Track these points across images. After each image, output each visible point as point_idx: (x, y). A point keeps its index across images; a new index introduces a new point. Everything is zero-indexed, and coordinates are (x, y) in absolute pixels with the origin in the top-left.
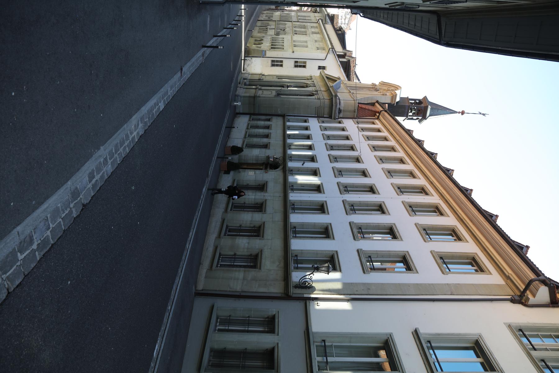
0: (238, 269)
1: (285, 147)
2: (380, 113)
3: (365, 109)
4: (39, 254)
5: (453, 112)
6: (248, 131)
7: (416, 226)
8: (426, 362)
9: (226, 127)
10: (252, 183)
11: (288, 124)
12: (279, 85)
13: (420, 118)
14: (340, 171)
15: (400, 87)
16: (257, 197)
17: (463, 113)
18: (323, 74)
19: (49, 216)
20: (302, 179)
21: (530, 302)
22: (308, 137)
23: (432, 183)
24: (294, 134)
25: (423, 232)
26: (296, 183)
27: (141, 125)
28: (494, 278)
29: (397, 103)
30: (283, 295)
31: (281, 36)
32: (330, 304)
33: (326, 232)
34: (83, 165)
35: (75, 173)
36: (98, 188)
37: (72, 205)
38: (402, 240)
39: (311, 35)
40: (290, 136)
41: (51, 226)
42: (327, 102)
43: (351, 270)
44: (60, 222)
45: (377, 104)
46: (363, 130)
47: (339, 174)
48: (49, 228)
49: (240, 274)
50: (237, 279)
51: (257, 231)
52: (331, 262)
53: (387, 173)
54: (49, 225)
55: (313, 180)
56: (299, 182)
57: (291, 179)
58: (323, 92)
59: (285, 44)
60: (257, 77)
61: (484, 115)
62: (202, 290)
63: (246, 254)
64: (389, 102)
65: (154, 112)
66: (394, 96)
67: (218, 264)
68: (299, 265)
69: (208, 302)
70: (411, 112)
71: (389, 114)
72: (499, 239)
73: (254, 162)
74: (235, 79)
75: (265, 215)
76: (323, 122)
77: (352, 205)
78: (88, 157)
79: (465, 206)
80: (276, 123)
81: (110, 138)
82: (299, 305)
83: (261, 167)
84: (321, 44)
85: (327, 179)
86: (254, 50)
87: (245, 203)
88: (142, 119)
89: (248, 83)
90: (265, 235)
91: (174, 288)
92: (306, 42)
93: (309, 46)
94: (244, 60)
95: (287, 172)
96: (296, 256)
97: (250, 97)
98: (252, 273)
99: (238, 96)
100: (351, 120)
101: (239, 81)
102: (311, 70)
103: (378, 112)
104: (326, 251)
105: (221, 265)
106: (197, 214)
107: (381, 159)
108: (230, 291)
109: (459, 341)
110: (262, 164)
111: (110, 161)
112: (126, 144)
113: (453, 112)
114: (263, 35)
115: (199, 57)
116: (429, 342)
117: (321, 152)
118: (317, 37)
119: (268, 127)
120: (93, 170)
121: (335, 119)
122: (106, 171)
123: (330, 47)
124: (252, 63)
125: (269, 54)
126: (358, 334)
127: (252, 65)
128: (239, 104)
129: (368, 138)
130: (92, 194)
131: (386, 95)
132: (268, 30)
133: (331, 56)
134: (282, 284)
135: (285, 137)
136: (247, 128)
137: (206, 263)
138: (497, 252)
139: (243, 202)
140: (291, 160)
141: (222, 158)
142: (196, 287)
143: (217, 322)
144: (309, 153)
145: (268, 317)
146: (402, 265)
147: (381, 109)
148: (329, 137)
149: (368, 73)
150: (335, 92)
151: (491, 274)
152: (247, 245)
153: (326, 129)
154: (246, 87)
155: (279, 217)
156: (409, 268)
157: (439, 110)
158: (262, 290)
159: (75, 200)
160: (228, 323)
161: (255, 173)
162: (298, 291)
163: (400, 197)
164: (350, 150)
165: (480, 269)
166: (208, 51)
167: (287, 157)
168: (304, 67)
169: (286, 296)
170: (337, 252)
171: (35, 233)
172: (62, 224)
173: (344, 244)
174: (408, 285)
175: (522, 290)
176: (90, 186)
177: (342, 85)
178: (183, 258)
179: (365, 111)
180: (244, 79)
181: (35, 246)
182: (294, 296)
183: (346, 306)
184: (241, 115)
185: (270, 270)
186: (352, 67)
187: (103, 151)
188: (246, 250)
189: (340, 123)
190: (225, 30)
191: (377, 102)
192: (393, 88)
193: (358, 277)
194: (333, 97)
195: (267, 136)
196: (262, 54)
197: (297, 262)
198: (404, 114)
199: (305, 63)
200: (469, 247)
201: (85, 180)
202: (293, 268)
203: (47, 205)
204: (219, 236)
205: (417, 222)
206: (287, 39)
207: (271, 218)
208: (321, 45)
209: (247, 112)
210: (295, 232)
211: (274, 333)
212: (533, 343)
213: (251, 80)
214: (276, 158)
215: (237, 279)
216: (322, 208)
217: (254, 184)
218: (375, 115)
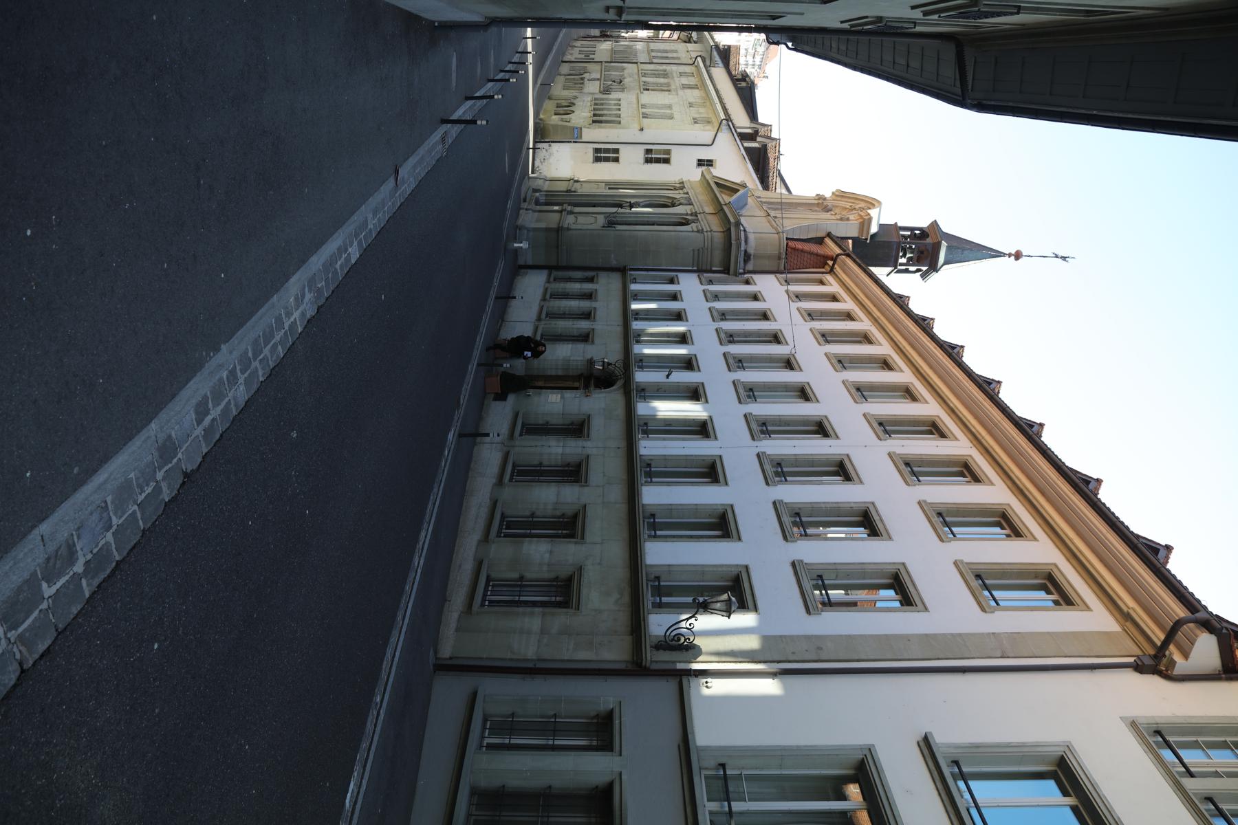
0: (529, 610)
1: (629, 338)
2: (834, 259)
3: (802, 251)
6: (546, 304)
9: (496, 298)
10: (554, 421)
12: (612, 203)
13: (924, 268)
14: (751, 390)
15: (879, 202)
16: (568, 450)
18: (708, 177)
19: (109, 499)
20: (667, 409)
21: (1177, 671)
22: (678, 316)
23: (953, 411)
24: (648, 311)
25: (937, 521)
26: (653, 418)
27: (308, 296)
28: (1095, 619)
29: (873, 236)
30: (630, 667)
31: (614, 96)
32: (735, 683)
33: (721, 525)
36: (218, 437)
38: (890, 538)
39: (681, 92)
40: (638, 315)
41: (115, 521)
42: (718, 237)
43: (779, 609)
44: (134, 512)
45: (828, 241)
46: (799, 297)
47: (749, 397)
48: (110, 527)
49: (533, 621)
50: (527, 634)
51: (569, 526)
52: (735, 591)
53: (853, 391)
57: (642, 409)
58: (709, 217)
59: (623, 113)
60: (562, 187)
61: (1064, 258)
62: (451, 658)
63: (546, 576)
64: (855, 234)
65: (338, 266)
66: (866, 222)
67: (484, 600)
68: (664, 600)
71: (854, 261)
72: (1104, 531)
73: (560, 373)
74: (514, 191)
75: (586, 490)
76: (711, 282)
78: (193, 369)
80: (607, 286)
81: (241, 325)
82: (666, 688)
83: (576, 384)
84: (702, 110)
85: (722, 408)
86: (555, 126)
87: (541, 464)
88: (311, 282)
89: (542, 199)
90: (587, 534)
91: (389, 655)
92: (670, 107)
94: (534, 149)
95: (632, 393)
96: (658, 578)
97: (547, 230)
98: (561, 619)
99: (521, 228)
100: (772, 277)
101: (523, 196)
102: (682, 170)
103: (832, 259)
105: (490, 602)
106: (435, 490)
107: (840, 361)
108: (511, 660)
109: (1023, 759)
110: (578, 377)
111: (243, 377)
112: (277, 338)
114: (574, 93)
115: (434, 144)
116: (956, 763)
117: (708, 349)
118: (694, 95)
119: (589, 296)
120: (205, 398)
121: (736, 274)
123: (723, 116)
124: (551, 155)
126: (798, 748)
127: (551, 160)
129: (811, 315)
130: (205, 450)
131: (848, 219)
133: (725, 138)
134: (628, 639)
135: (627, 316)
136: (544, 299)
137: (458, 599)
139: (536, 462)
140: (641, 368)
142: (436, 652)
143: (484, 728)
144: (681, 351)
146: (891, 593)
147: (838, 251)
148: (723, 316)
149: (806, 172)
151: (1088, 609)
152: (547, 555)
153: (716, 297)
154: (538, 208)
155: (617, 493)
156: (907, 600)
157: (966, 250)
159: (166, 464)
160: (508, 728)
163: (883, 443)
165: (1065, 599)
166: (454, 130)
168: (667, 161)
169: (637, 668)
170: (747, 567)
171: (79, 538)
172: (139, 515)
173: (761, 551)
174: (907, 638)
175: (1159, 644)
176: (199, 431)
177: (750, 200)
178: (408, 587)
179: (803, 257)
180: (535, 191)
181: (79, 568)
182: (654, 667)
183: (770, 687)
186: (771, 160)
187: (227, 356)
188: (545, 568)
189: (747, 282)
191: (829, 235)
192: (862, 205)
194: (731, 228)
196: (573, 136)
197: (659, 591)
198: (888, 260)
199: (668, 152)
200: (1038, 551)
201: (188, 420)
204: (486, 539)
206: (627, 101)
207: (600, 497)
208: (703, 112)
209: (542, 263)
210: (654, 526)
211: (612, 750)
212: (1186, 761)
214: (609, 364)
215: (527, 634)
216: (721, 525)
217: (561, 422)
218: (824, 263)
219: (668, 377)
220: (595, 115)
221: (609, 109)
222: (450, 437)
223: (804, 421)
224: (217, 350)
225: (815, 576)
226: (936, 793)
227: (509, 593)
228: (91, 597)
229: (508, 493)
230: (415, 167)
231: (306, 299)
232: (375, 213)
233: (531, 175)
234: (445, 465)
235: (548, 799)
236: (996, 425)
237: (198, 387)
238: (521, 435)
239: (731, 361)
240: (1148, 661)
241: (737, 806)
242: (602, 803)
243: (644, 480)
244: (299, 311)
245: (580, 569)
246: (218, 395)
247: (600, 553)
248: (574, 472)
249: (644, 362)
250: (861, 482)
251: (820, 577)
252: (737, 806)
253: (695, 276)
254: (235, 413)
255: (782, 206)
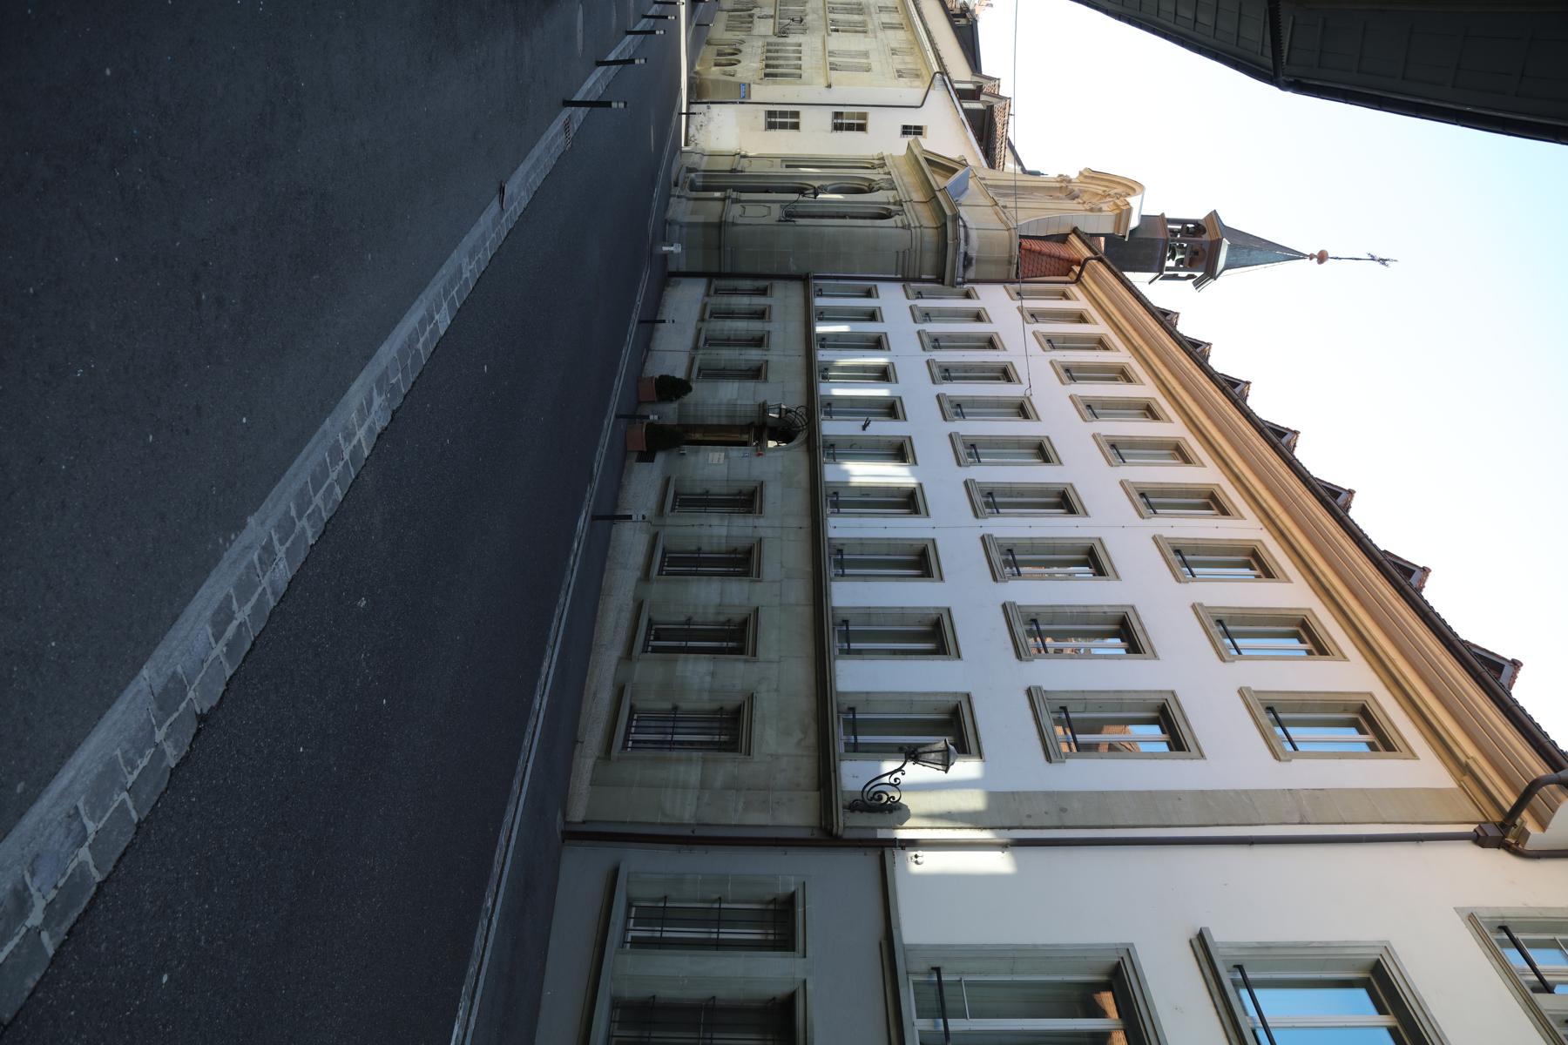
0: (684, 754)
1: (813, 373)
2: (1083, 264)
3: (1040, 253)
4: (51, 938)
5: (1292, 255)
6: (705, 326)
7: (1197, 613)
8: (1232, 1034)
9: (640, 322)
10: (717, 489)
11: (820, 302)
12: (791, 187)
13: (1198, 274)
14: (973, 446)
15: (1141, 186)
16: (735, 531)
17: (1322, 257)
18: (916, 151)
19: (81, 805)
20: (864, 473)
21: (1530, 845)
22: (878, 343)
23: (1238, 478)
24: (838, 335)
25: (1216, 630)
26: (846, 486)
27: (378, 401)
28: (1423, 771)
29: (1133, 231)
30: (817, 835)
31: (792, 39)
32: (954, 862)
33: (935, 636)
34: (187, 600)
35: (165, 633)
36: (248, 646)
37: (159, 736)
38: (1155, 657)
39: (880, 34)
40: (827, 341)
41: (91, 827)
42: (930, 236)
43: (1010, 755)
44: (123, 802)
45: (1073, 239)
46: (1035, 316)
47: (970, 455)
48: (85, 838)
49: (689, 770)
50: (683, 788)
51: (741, 562)
52: (952, 729)
53: (1107, 448)
54: (84, 828)
55: (893, 474)
56: (856, 481)
57: (830, 473)
58: (919, 207)
59: (805, 63)
60: (725, 165)
61: (1383, 261)
62: (584, 822)
63: (707, 706)
64: (1109, 230)
65: (420, 346)
66: (1123, 214)
67: (626, 740)
68: (854, 646)
69: (604, 855)
70: (1173, 257)
71: (1109, 268)
72: (1438, 652)
73: (724, 421)
74: (661, 174)
75: (758, 586)
76: (920, 295)
77: (1010, 551)
78: (202, 571)
79: (1338, 549)
80: (784, 301)
81: (276, 479)
82: (864, 862)
83: (745, 437)
84: (908, 59)
85: (935, 472)
86: (716, 82)
87: (699, 550)
88: (381, 382)
89: (699, 182)
90: (760, 648)
91: (502, 840)
92: (866, 54)
93: (875, 66)
94: (688, 114)
95: (818, 451)
96: (852, 710)
97: (706, 225)
98: (727, 767)
99: (671, 223)
100: (999, 288)
101: (673, 177)
102: (882, 140)
103: (1078, 263)
104: (936, 694)
105: (634, 742)
106: (561, 600)
107: (1089, 407)
108: (662, 824)
109: (1325, 964)
110: (746, 428)
111: (283, 549)
112: (333, 476)
113: (1292, 255)
114: (740, 35)
115: (553, 138)
116: (1240, 968)
117: (916, 388)
118: (898, 38)
119: (761, 315)
120: (228, 598)
121: (953, 284)
122: (272, 583)
123: (936, 68)
124: (710, 120)
125: (758, 93)
126: (1035, 948)
127: (712, 126)
128: (676, 249)
129: (1051, 342)
130: (229, 673)
131: (1100, 210)
132: (756, 20)
133: (939, 97)
134: (814, 796)
135: (811, 342)
136: (702, 320)
137: (593, 738)
138: (1433, 690)
139: (693, 548)
140: (830, 414)
141: (630, 417)
142: (564, 815)
143: (628, 918)
144: (881, 391)
145: (774, 901)
146: (1155, 730)
147: (1088, 254)
148: (937, 342)
149: (1045, 142)
150: (953, 208)
151: (1414, 756)
152: (708, 679)
153: (927, 316)
154: (694, 194)
155: (798, 592)
156: (1177, 743)
157: (1256, 250)
158: (756, 818)
159: (169, 715)
160: (661, 924)
161: (726, 457)
162: (860, 819)
163: (1146, 522)
164: (998, 379)
165: (1383, 743)
166: (581, 112)
167: (818, 406)
168: (862, 128)
169: (826, 837)
170: (968, 696)
171: (33, 874)
172: (130, 804)
173: (986, 673)
174: (1176, 796)
175: (1508, 809)
176: (220, 649)
177: (971, 182)
178: (526, 743)
179: (1040, 261)
180: (690, 170)
181: (36, 918)
182: (848, 835)
183: (998, 862)
184: (684, 280)
185: (776, 757)
186: (999, 126)
187: (258, 528)
188: (705, 696)
189: (968, 295)
190: (629, 37)
191: (1075, 231)
192: (1119, 190)
193: (1032, 773)
194: (946, 223)
195: (759, 342)
196: (740, 95)
197: (854, 726)
198: (1151, 263)
199: (864, 116)
200: (1348, 675)
201: (196, 648)
202: (837, 652)
203: (72, 773)
204: (628, 655)
205: (1198, 601)
206: (810, 46)
207: (776, 595)
208: (909, 62)
209: (699, 268)
210: (841, 564)
211: (793, 949)
212: (1539, 967)
213: (709, 174)
214: (788, 411)
215: (683, 788)
216: (921, 562)
217: (725, 491)
218: (1068, 269)
219: (864, 428)
220: (767, 66)
221: (786, 58)
222: (581, 523)
223: (1043, 490)
224: (240, 526)
225: (1057, 708)
226: (1213, 1010)
227: (656, 730)
228: (58, 953)
229: (658, 590)
230: (528, 175)
231: (375, 407)
232: (471, 257)
233: (685, 149)
234: (574, 562)
235: (711, 1014)
236: (1295, 500)
237: (216, 588)
238: (673, 510)
239: (947, 406)
240: (1492, 832)
241: (956, 1025)
242: (781, 1018)
243: (833, 571)
244: (365, 426)
245: (751, 697)
246: (245, 588)
247: (776, 595)
248: (742, 562)
249: (835, 408)
250: (1118, 578)
251: (1064, 709)
252: (956, 1025)
253: (899, 286)
254: (272, 603)
255: (1016, 191)
